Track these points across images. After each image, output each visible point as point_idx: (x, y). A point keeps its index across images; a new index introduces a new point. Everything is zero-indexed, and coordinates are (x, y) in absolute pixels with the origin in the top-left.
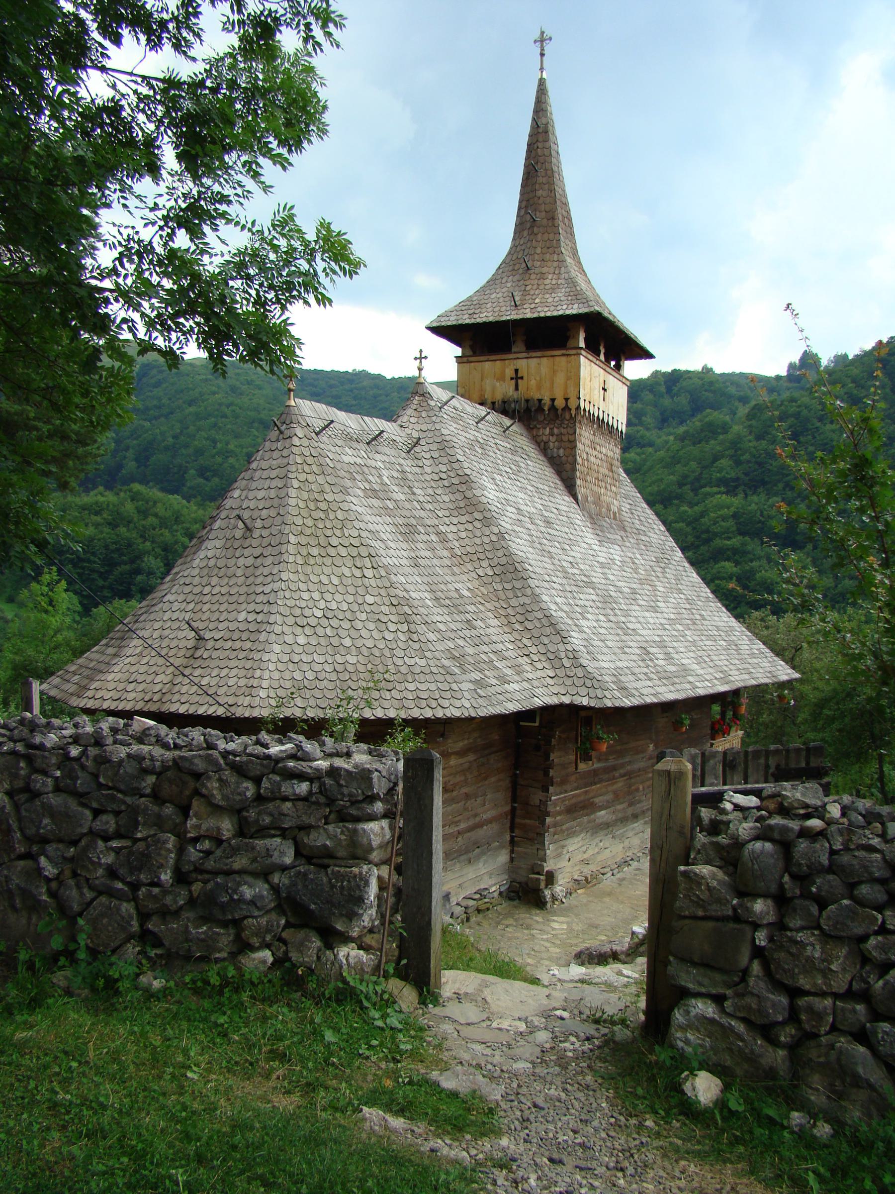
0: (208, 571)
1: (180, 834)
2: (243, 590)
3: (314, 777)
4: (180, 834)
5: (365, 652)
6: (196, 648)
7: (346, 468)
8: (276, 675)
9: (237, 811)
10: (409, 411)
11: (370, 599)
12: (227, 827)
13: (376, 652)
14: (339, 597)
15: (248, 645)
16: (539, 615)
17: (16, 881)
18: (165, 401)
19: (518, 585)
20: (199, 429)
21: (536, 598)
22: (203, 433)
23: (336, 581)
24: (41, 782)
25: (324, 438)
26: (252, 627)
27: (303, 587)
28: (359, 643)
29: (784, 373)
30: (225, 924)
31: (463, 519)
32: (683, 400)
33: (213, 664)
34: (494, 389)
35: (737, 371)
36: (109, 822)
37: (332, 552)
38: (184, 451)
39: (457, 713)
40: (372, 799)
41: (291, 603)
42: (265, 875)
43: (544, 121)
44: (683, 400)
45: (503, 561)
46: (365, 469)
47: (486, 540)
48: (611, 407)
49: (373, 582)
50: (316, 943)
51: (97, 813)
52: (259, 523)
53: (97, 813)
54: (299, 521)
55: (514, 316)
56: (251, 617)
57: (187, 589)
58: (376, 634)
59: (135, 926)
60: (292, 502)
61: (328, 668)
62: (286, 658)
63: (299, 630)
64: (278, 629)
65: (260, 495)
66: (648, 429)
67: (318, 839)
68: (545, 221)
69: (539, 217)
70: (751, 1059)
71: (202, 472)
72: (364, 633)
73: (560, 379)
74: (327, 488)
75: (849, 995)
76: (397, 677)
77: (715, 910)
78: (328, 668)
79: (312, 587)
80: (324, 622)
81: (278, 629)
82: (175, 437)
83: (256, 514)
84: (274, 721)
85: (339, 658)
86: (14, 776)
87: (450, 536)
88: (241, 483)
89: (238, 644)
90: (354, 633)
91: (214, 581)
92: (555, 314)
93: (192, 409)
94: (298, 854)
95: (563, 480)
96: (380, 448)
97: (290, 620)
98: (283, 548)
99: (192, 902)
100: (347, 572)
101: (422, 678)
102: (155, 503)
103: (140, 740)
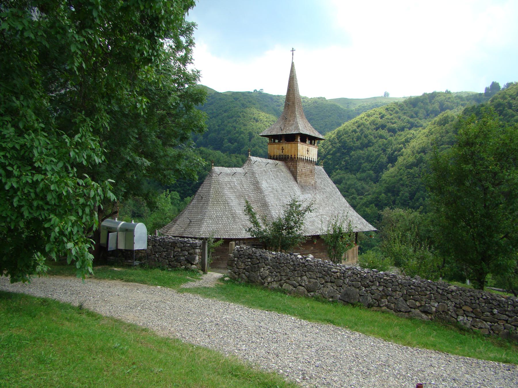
0: (193, 207)
1: (174, 251)
2: (200, 211)
3: (190, 244)
4: (174, 251)
5: (224, 224)
6: (190, 223)
7: (225, 182)
8: (204, 229)
9: (181, 248)
10: (246, 165)
11: (226, 213)
12: (180, 250)
13: (226, 224)
14: (220, 213)
15: (200, 223)
16: (270, 216)
17: (153, 258)
18: (215, 111)
19: (266, 208)
20: (229, 123)
21: (270, 211)
22: (230, 124)
23: (219, 209)
24: (157, 245)
25: (220, 176)
26: (201, 219)
27: (212, 210)
28: (222, 223)
29: (483, 91)
30: (179, 262)
31: (256, 192)
32: (437, 106)
33: (192, 227)
34: (277, 152)
35: (464, 91)
36: (165, 250)
37: (219, 203)
38: (223, 132)
39: (241, 237)
40: (197, 246)
41: (209, 214)
42: (184, 256)
43: (293, 75)
44: (437, 106)
45: (263, 202)
46: (230, 182)
47: (260, 197)
48: (311, 155)
49: (228, 209)
50: (190, 265)
51: (164, 248)
52: (204, 196)
53: (164, 248)
54: (212, 196)
55: (280, 133)
56: (201, 217)
57: (189, 210)
58: (226, 221)
59: (168, 263)
60: (211, 192)
61: (215, 228)
62: (207, 226)
63: (210, 220)
64: (206, 220)
65: (205, 190)
66: (420, 119)
67: (190, 252)
68: (292, 105)
69: (290, 103)
70: (234, 276)
71: (230, 141)
72: (224, 220)
73: (293, 150)
74: (219, 188)
75: (244, 269)
76: (230, 230)
77: (231, 259)
78: (215, 228)
79: (214, 210)
80: (216, 218)
81: (206, 220)
82: (219, 126)
83: (204, 194)
84: (199, 238)
85: (218, 226)
86: (153, 243)
87: (252, 197)
88: (201, 187)
89: (198, 223)
90: (222, 221)
91: (195, 209)
92: (291, 133)
93: (226, 114)
94: (188, 254)
95: (294, 177)
96: (236, 176)
97: (209, 218)
98: (209, 202)
99: (175, 260)
100: (222, 207)
101: (235, 230)
102: (209, 155)
103: (169, 239)
